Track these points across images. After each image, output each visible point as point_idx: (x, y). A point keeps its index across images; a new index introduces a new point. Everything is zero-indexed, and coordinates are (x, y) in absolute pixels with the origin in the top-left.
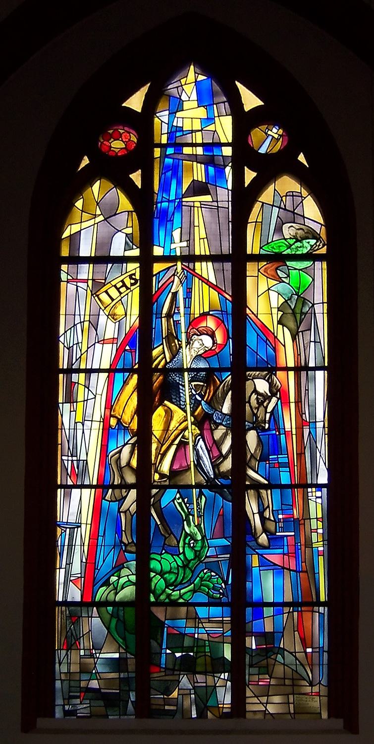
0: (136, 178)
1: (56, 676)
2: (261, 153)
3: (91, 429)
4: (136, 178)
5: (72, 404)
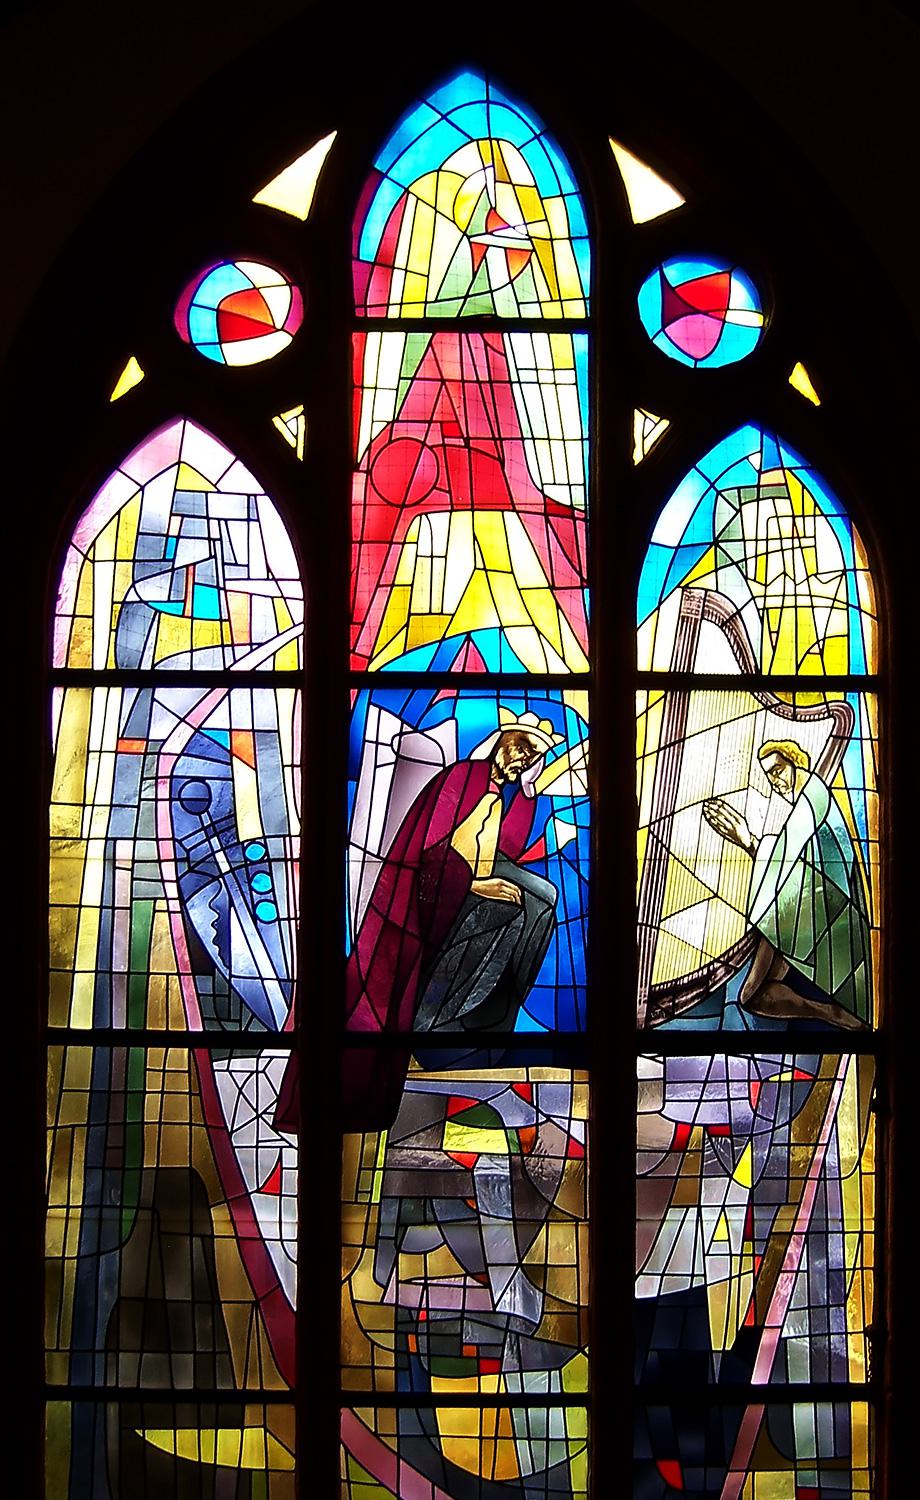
1: (49, 1244)
2: (67, 551)
3: (86, 859)
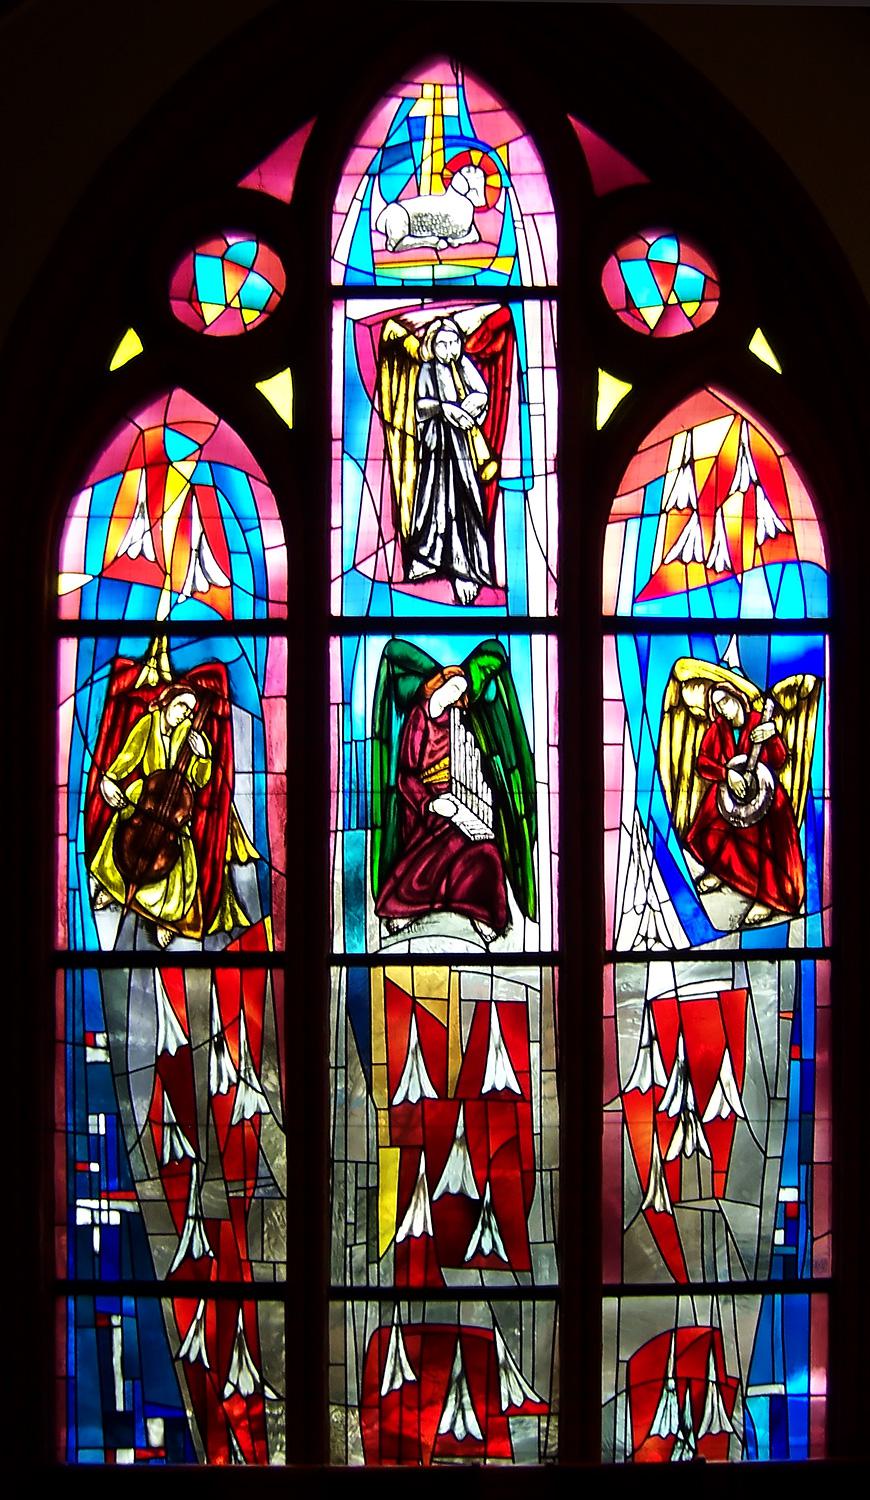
0: (278, 391)
4: (278, 391)
5: (369, 832)
